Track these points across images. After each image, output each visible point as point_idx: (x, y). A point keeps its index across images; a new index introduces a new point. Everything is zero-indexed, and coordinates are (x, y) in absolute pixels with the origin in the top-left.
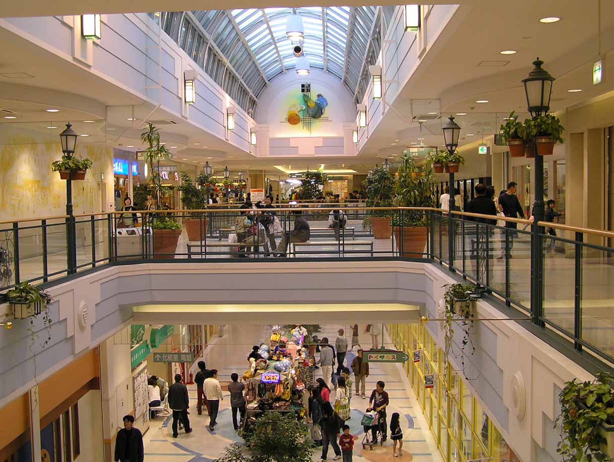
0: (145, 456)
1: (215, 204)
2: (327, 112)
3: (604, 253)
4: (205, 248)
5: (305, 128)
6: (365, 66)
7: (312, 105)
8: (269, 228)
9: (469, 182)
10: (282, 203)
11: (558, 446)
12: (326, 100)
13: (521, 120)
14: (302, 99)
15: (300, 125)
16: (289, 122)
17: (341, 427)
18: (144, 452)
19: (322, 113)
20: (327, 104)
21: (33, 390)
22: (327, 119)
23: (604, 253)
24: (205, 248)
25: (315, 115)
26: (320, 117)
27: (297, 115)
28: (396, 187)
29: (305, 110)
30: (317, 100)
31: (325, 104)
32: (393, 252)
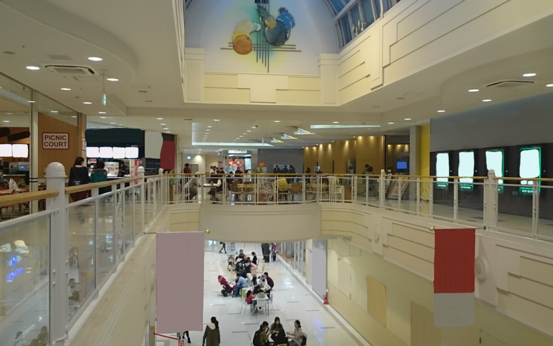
0: (204, 282)
1: (413, 138)
2: (294, 38)
3: (231, 276)
5: (260, 61)
7: (271, 24)
8: (240, 170)
11: (287, 333)
15: (253, 54)
16: (236, 50)
17: (546, 86)
18: (205, 280)
19: (286, 39)
20: (294, 24)
22: (293, 49)
23: (231, 276)
26: (283, 44)
27: (248, 38)
29: (260, 30)
30: (279, 17)
31: (291, 24)
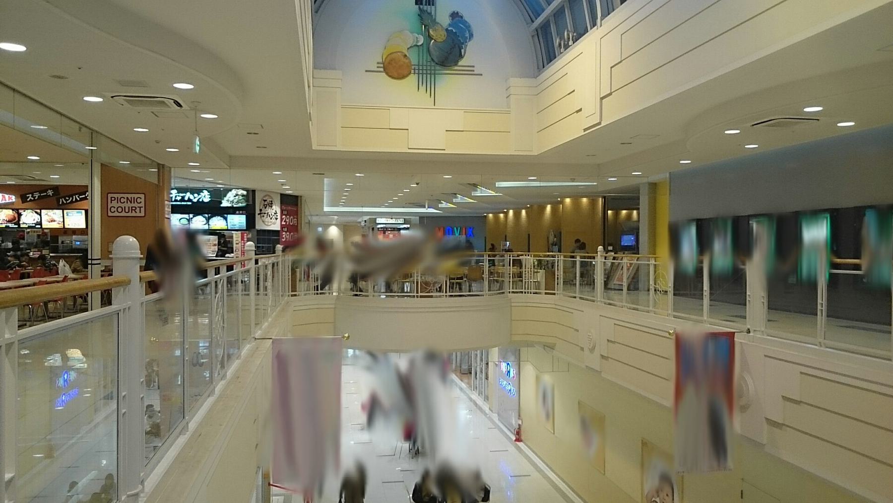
4: (423, 76)
6: (263, 284)
7: (439, 35)
9: (190, 322)
10: (534, 272)
12: (470, 26)
13: (462, 241)
14: (415, 19)
15: (412, 79)
16: (387, 74)
20: (471, 36)
21: (550, 18)
22: (470, 71)
24: (423, 76)
25: (447, 58)
27: (405, 56)
28: (586, 268)
30: (450, 25)
31: (467, 35)
32: (92, 264)
